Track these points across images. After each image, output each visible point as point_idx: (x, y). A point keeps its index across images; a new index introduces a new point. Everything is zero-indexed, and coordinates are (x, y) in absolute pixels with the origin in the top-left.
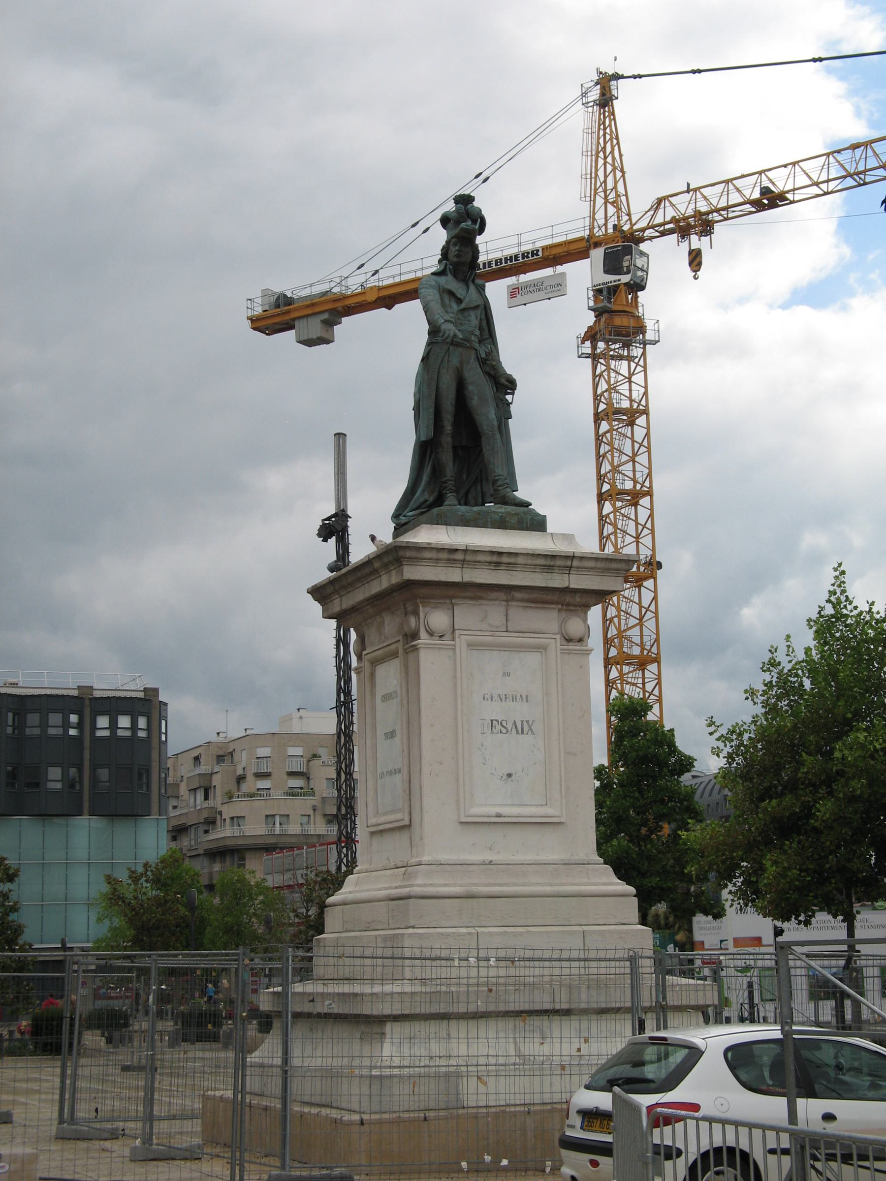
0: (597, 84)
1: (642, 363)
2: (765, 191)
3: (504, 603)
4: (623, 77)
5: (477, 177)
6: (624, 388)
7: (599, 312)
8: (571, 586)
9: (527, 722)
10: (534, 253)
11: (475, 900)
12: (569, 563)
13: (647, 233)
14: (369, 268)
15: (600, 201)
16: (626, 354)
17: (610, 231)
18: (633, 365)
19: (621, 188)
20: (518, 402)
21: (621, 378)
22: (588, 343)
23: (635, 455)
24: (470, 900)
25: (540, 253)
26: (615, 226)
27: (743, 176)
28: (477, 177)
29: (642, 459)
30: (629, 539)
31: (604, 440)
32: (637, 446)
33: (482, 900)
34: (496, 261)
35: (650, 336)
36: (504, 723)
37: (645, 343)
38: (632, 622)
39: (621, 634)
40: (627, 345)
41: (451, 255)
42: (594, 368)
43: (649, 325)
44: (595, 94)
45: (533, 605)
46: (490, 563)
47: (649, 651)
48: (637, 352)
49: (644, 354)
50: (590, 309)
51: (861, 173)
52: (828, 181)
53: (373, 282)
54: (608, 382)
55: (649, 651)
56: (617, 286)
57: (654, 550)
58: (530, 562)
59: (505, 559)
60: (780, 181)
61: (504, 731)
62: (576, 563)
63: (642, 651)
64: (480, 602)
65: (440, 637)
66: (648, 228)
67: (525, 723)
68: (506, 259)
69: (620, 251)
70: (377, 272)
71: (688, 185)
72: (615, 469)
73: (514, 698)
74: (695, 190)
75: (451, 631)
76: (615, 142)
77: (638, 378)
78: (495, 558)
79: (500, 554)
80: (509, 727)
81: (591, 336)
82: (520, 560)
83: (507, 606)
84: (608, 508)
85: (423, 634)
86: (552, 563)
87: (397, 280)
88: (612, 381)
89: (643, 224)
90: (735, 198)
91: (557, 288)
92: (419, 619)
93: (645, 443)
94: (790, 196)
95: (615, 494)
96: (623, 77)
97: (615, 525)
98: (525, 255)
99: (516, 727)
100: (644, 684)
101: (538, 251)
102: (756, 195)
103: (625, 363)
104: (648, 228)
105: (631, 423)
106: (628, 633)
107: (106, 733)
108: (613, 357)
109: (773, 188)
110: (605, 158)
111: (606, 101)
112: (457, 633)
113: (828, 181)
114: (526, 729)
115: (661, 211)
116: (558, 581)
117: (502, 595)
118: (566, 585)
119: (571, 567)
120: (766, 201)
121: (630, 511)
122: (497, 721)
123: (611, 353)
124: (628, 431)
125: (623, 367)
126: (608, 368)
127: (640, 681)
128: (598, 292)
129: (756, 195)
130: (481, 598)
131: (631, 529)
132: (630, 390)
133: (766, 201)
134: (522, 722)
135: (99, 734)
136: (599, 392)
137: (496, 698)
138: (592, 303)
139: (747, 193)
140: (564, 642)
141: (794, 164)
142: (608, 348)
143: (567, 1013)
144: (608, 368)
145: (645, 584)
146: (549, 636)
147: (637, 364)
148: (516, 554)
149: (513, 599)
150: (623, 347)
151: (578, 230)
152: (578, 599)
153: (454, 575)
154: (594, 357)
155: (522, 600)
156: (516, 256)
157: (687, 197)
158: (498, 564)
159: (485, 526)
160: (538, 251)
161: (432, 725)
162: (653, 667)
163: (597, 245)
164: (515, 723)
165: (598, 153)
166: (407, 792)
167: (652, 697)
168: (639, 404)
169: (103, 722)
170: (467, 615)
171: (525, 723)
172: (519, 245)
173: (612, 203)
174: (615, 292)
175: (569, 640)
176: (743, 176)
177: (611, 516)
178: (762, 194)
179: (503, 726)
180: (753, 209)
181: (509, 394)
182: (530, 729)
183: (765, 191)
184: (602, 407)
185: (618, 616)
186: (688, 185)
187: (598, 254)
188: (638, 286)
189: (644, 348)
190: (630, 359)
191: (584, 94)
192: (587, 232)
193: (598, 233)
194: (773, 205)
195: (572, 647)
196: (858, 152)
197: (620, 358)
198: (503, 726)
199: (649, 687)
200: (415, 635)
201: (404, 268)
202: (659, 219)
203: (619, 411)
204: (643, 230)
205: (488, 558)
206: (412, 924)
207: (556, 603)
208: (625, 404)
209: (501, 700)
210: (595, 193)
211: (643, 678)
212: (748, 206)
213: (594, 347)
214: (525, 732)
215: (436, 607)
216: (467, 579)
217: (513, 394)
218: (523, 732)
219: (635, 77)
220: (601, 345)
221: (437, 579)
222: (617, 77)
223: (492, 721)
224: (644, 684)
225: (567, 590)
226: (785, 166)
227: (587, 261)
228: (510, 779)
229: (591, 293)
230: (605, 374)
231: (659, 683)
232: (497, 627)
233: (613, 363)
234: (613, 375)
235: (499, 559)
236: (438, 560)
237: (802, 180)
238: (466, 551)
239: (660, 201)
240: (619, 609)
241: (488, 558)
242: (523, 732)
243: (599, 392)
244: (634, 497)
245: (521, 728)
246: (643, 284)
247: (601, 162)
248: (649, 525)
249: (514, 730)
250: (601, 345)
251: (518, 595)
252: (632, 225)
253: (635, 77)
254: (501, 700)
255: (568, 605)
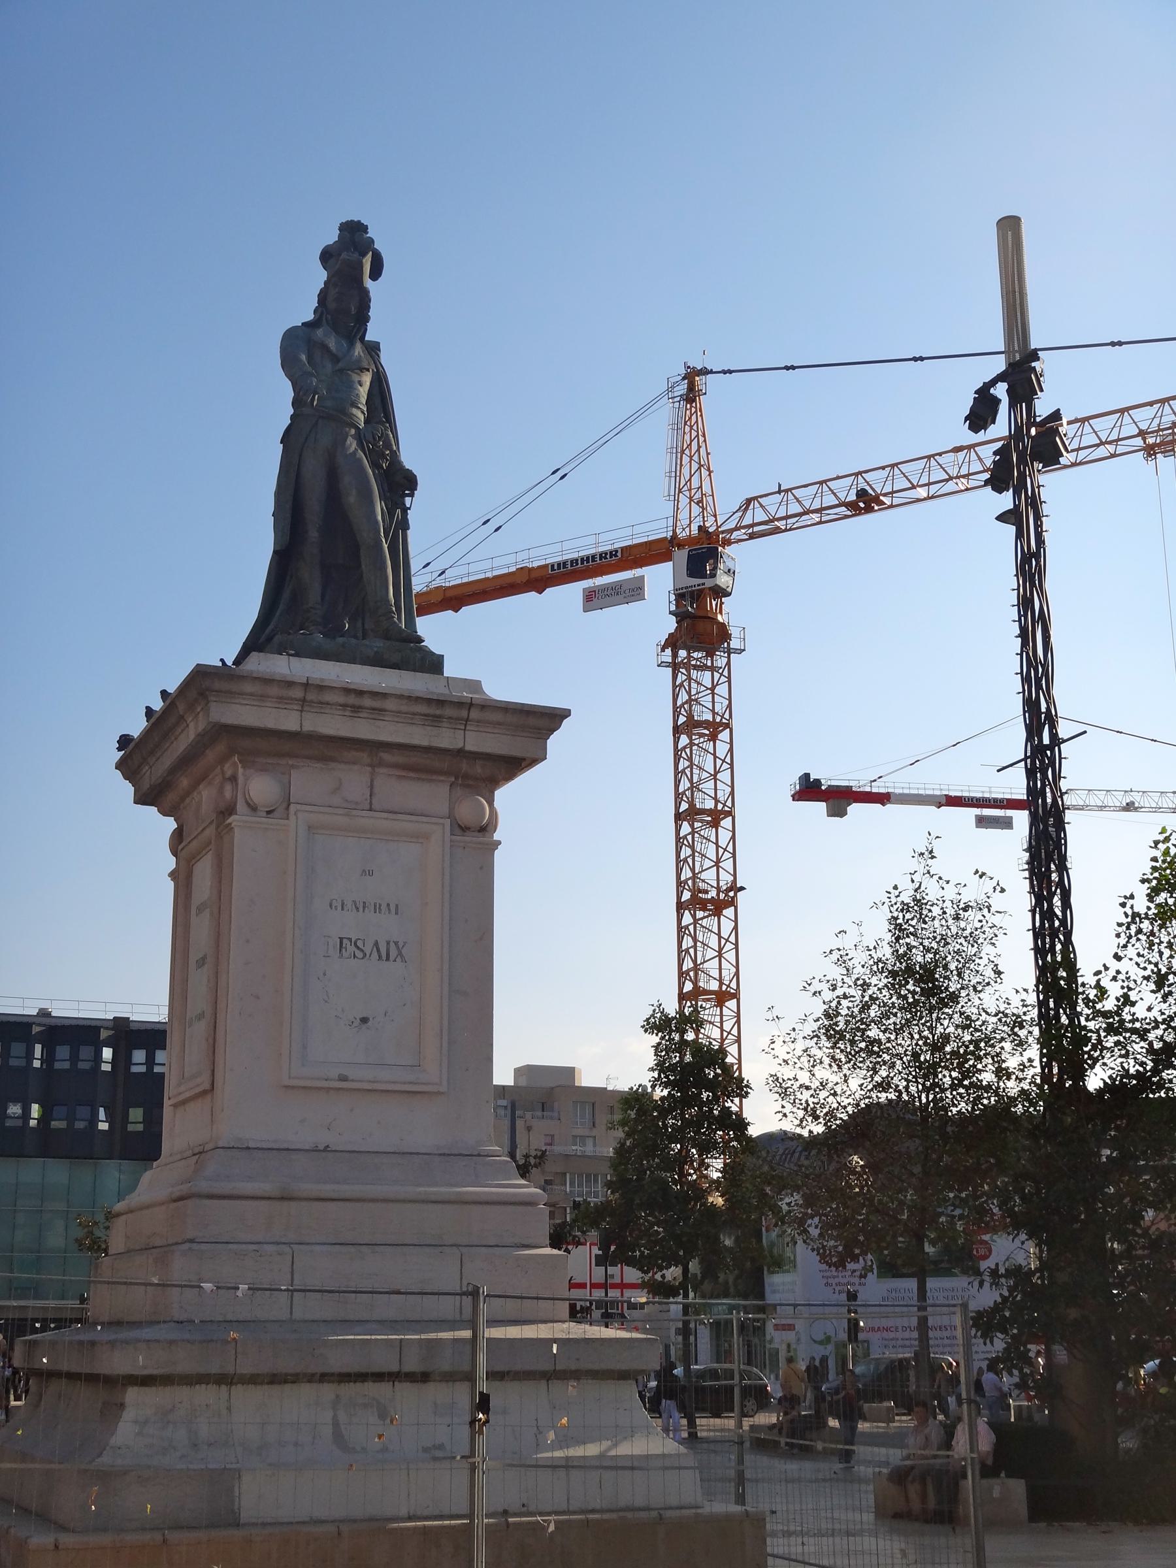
0: (684, 379)
1: (726, 673)
2: (862, 494)
3: (369, 769)
4: (711, 372)
5: (554, 473)
6: (707, 700)
7: (680, 616)
8: (468, 748)
9: (396, 943)
10: (613, 553)
11: (293, 1204)
12: (464, 713)
13: (735, 535)
14: (436, 567)
15: (684, 500)
16: (709, 664)
17: (695, 531)
18: (717, 675)
19: (706, 488)
20: (418, 508)
21: (703, 688)
22: (668, 651)
23: (716, 772)
24: (286, 1203)
25: (619, 554)
26: (700, 527)
27: (838, 478)
28: (554, 473)
29: (725, 776)
30: (707, 864)
31: (684, 755)
32: (719, 762)
33: (304, 1203)
34: (572, 562)
35: (735, 644)
36: (360, 944)
37: (729, 651)
38: (711, 953)
39: (696, 968)
40: (710, 654)
41: (332, 305)
42: (675, 678)
43: (734, 632)
44: (682, 388)
45: (411, 774)
46: (344, 706)
47: (728, 986)
48: (721, 661)
49: (728, 663)
50: (671, 613)
51: (963, 476)
52: (929, 484)
53: (439, 582)
54: (689, 693)
55: (728, 986)
56: (701, 591)
57: (735, 875)
58: (404, 708)
59: (367, 702)
60: (877, 482)
61: (359, 954)
62: (475, 714)
63: (720, 987)
64: (333, 765)
65: (269, 812)
66: (737, 529)
67: (392, 945)
68: (582, 559)
69: (702, 554)
70: (443, 572)
71: (780, 486)
72: (693, 787)
73: (377, 908)
74: (787, 491)
75: (285, 805)
76: (701, 439)
77: (722, 690)
78: (352, 700)
79: (360, 693)
80: (368, 951)
81: (672, 643)
82: (390, 705)
83: (372, 774)
84: (686, 828)
85: (241, 806)
86: (438, 712)
87: (465, 580)
88: (693, 692)
89: (731, 525)
90: (830, 500)
91: (635, 592)
92: (237, 785)
93: (728, 760)
94: (887, 501)
95: (693, 813)
96: (711, 372)
97: (692, 847)
98: (603, 555)
99: (378, 950)
100: (722, 1022)
101: (617, 552)
102: (852, 497)
103: (708, 674)
104: (737, 529)
105: (713, 738)
106: (705, 965)
107: (143, 1069)
108: (696, 667)
109: (871, 491)
110: (691, 457)
111: (692, 396)
112: (293, 808)
113: (929, 484)
114: (393, 952)
115: (750, 512)
116: (447, 738)
117: (364, 756)
118: (460, 745)
119: (467, 720)
120: (862, 505)
121: (710, 833)
122: (350, 940)
123: (693, 663)
124: (710, 746)
125: (706, 678)
126: (689, 678)
127: (718, 1019)
128: (680, 597)
129: (852, 497)
130: (332, 759)
131: (711, 852)
132: (713, 702)
133: (862, 505)
134: (388, 943)
135: (134, 1069)
136: (679, 703)
137: (349, 904)
138: (673, 608)
139: (842, 496)
140: (458, 831)
141: (893, 466)
142: (689, 657)
143: (423, 1377)
144: (689, 678)
145: (724, 912)
146: (434, 820)
147: (721, 674)
148: (384, 696)
149: (381, 764)
150: (707, 656)
151: (659, 530)
152: (478, 769)
153: (289, 721)
154: (675, 667)
155: (396, 766)
156: (593, 557)
157: (778, 497)
158: (356, 709)
159: (352, 661)
160: (617, 552)
161: (248, 941)
162: (732, 1004)
163: (681, 545)
164: (376, 944)
165: (683, 452)
166: (211, 1041)
167: (730, 1037)
168: (722, 717)
169: (139, 1056)
170: (308, 781)
171: (392, 945)
172: (597, 544)
173: (697, 503)
174: (699, 596)
175: (464, 829)
176: (838, 478)
177: (689, 838)
178: (858, 495)
179: (358, 948)
180: (849, 513)
181: (408, 495)
182: (400, 954)
183: (862, 494)
184: (682, 719)
185: (695, 947)
186: (780, 486)
187: (682, 555)
188: (721, 593)
189: (729, 657)
190: (713, 669)
191: (670, 389)
192: (671, 533)
193: (682, 535)
194: (869, 509)
195: (468, 838)
196: (961, 455)
197: (704, 668)
198: (358, 948)
199: (727, 1026)
200: (230, 810)
201: (473, 568)
202: (747, 520)
203: (700, 724)
204: (731, 531)
205: (341, 699)
206: (189, 1236)
207: (447, 773)
208: (708, 716)
209: (357, 909)
210: (680, 491)
211: (721, 1015)
212: (844, 509)
213: (675, 655)
214: (392, 958)
215: (263, 770)
216: (308, 727)
217: (412, 495)
218: (388, 959)
219: (724, 372)
220: (683, 653)
221: (262, 726)
222: (705, 372)
223: (341, 939)
224: (722, 1022)
225: (461, 753)
226: (883, 468)
227: (669, 565)
228: (364, 1027)
229: (673, 597)
230: (686, 684)
231: (738, 1022)
232: (357, 803)
233: (694, 674)
234: (694, 685)
235: (357, 701)
236: (263, 697)
237: (902, 483)
238: (307, 685)
239: (749, 501)
240: (695, 940)
241: (341, 699)
242: (388, 959)
243: (679, 703)
244: (716, 817)
245: (388, 952)
246: (729, 590)
247: (686, 459)
248: (730, 848)
249: (375, 954)
250: (683, 653)
251: (387, 757)
252: (718, 527)
253: (724, 372)
254: (357, 909)
255: (466, 776)
